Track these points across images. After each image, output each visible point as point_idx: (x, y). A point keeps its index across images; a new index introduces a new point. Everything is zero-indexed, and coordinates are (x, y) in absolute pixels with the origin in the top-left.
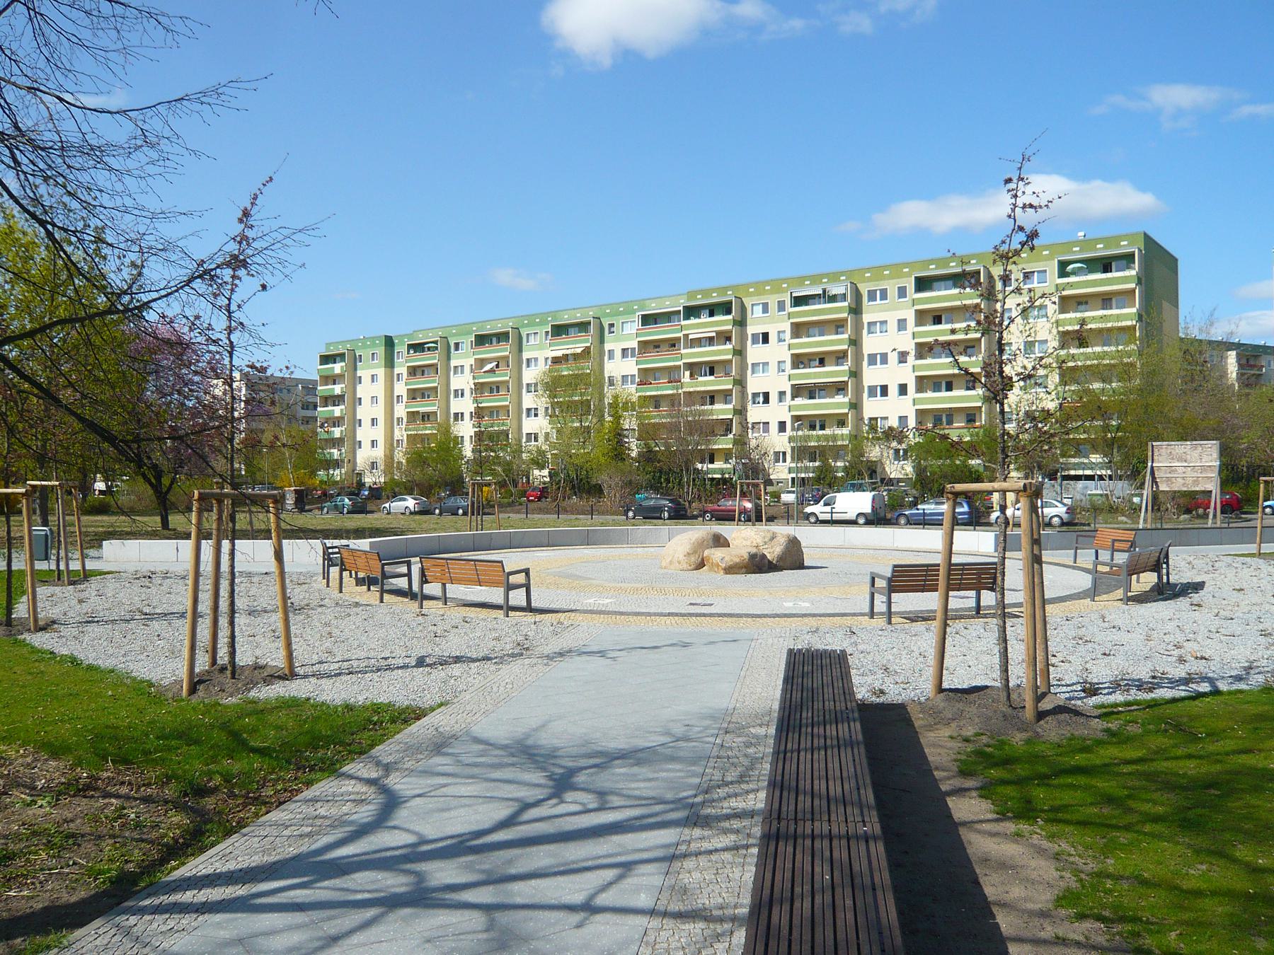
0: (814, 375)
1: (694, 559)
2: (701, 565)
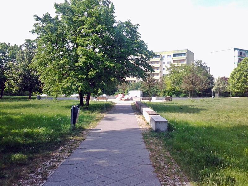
0: (177, 58)
1: (121, 99)
2: (121, 100)
